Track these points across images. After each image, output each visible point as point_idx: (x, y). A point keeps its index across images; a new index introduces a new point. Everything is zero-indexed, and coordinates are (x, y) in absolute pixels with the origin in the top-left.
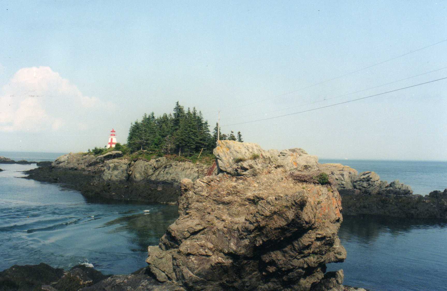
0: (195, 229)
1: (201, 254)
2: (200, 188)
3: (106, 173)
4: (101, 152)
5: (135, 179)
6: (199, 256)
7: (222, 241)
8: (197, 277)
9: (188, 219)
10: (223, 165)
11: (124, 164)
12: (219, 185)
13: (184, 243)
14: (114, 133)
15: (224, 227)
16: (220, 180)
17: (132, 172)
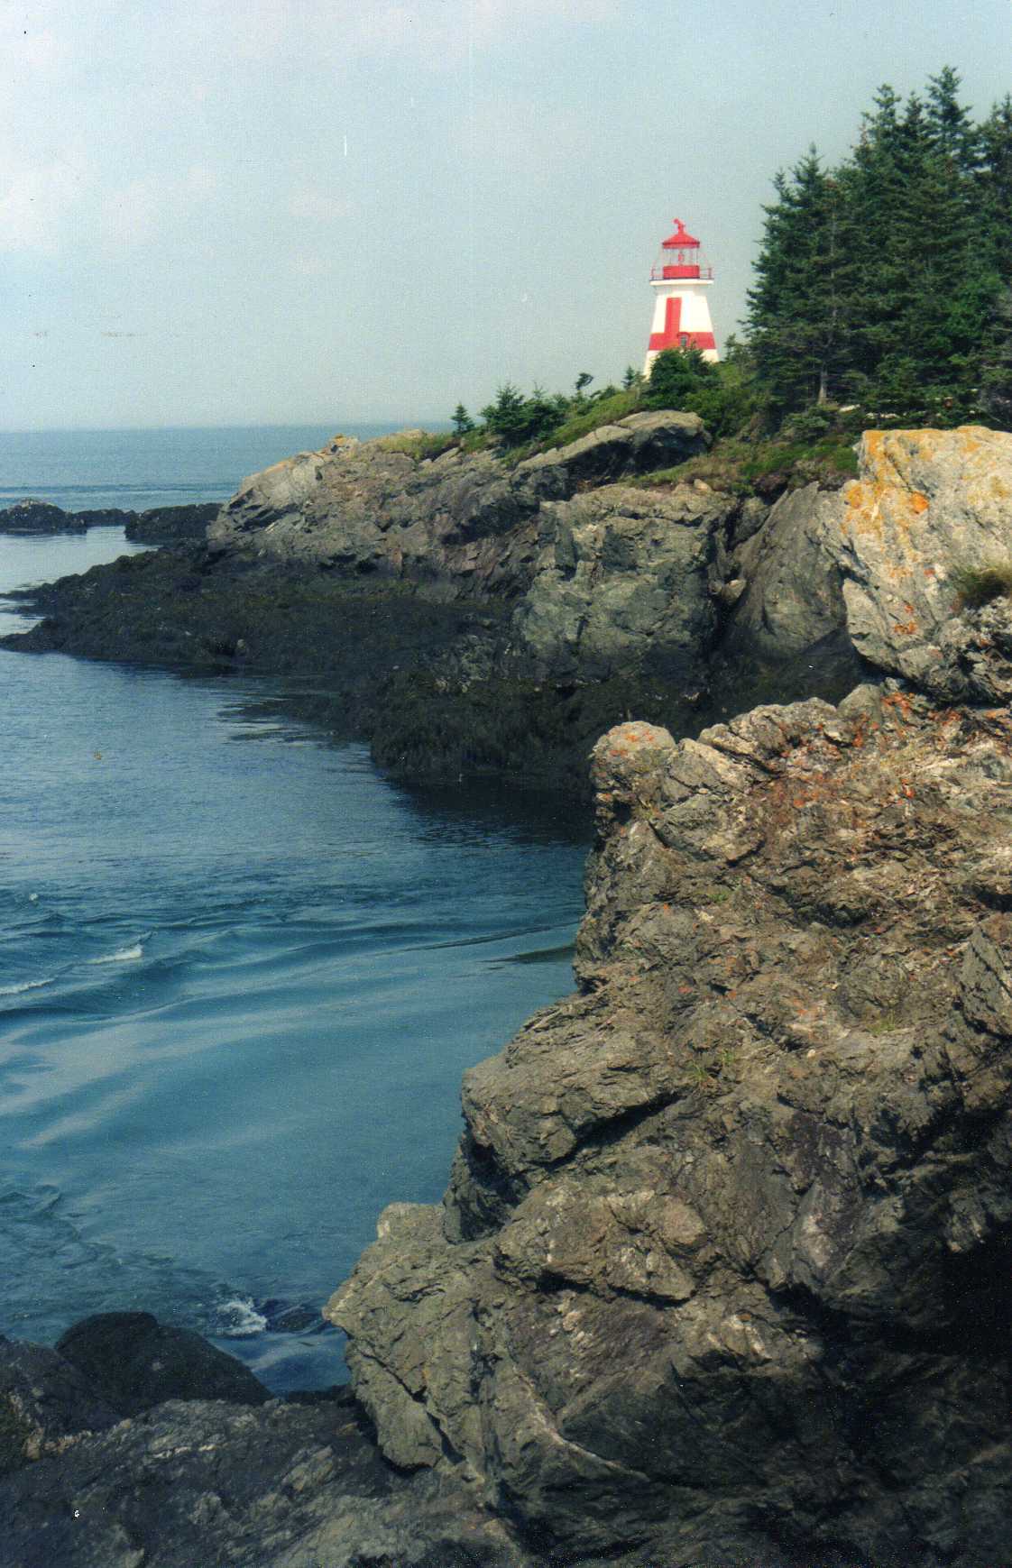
0: (599, 1105)
1: (619, 1284)
2: (698, 803)
3: (546, 596)
4: (550, 427)
5: (765, 638)
6: (610, 1301)
7: (763, 1200)
8: (575, 1447)
9: (578, 1026)
10: (877, 626)
11: (681, 521)
12: (842, 773)
13: (534, 1196)
14: (690, 257)
15: (782, 1099)
16: (847, 739)
17: (750, 579)
